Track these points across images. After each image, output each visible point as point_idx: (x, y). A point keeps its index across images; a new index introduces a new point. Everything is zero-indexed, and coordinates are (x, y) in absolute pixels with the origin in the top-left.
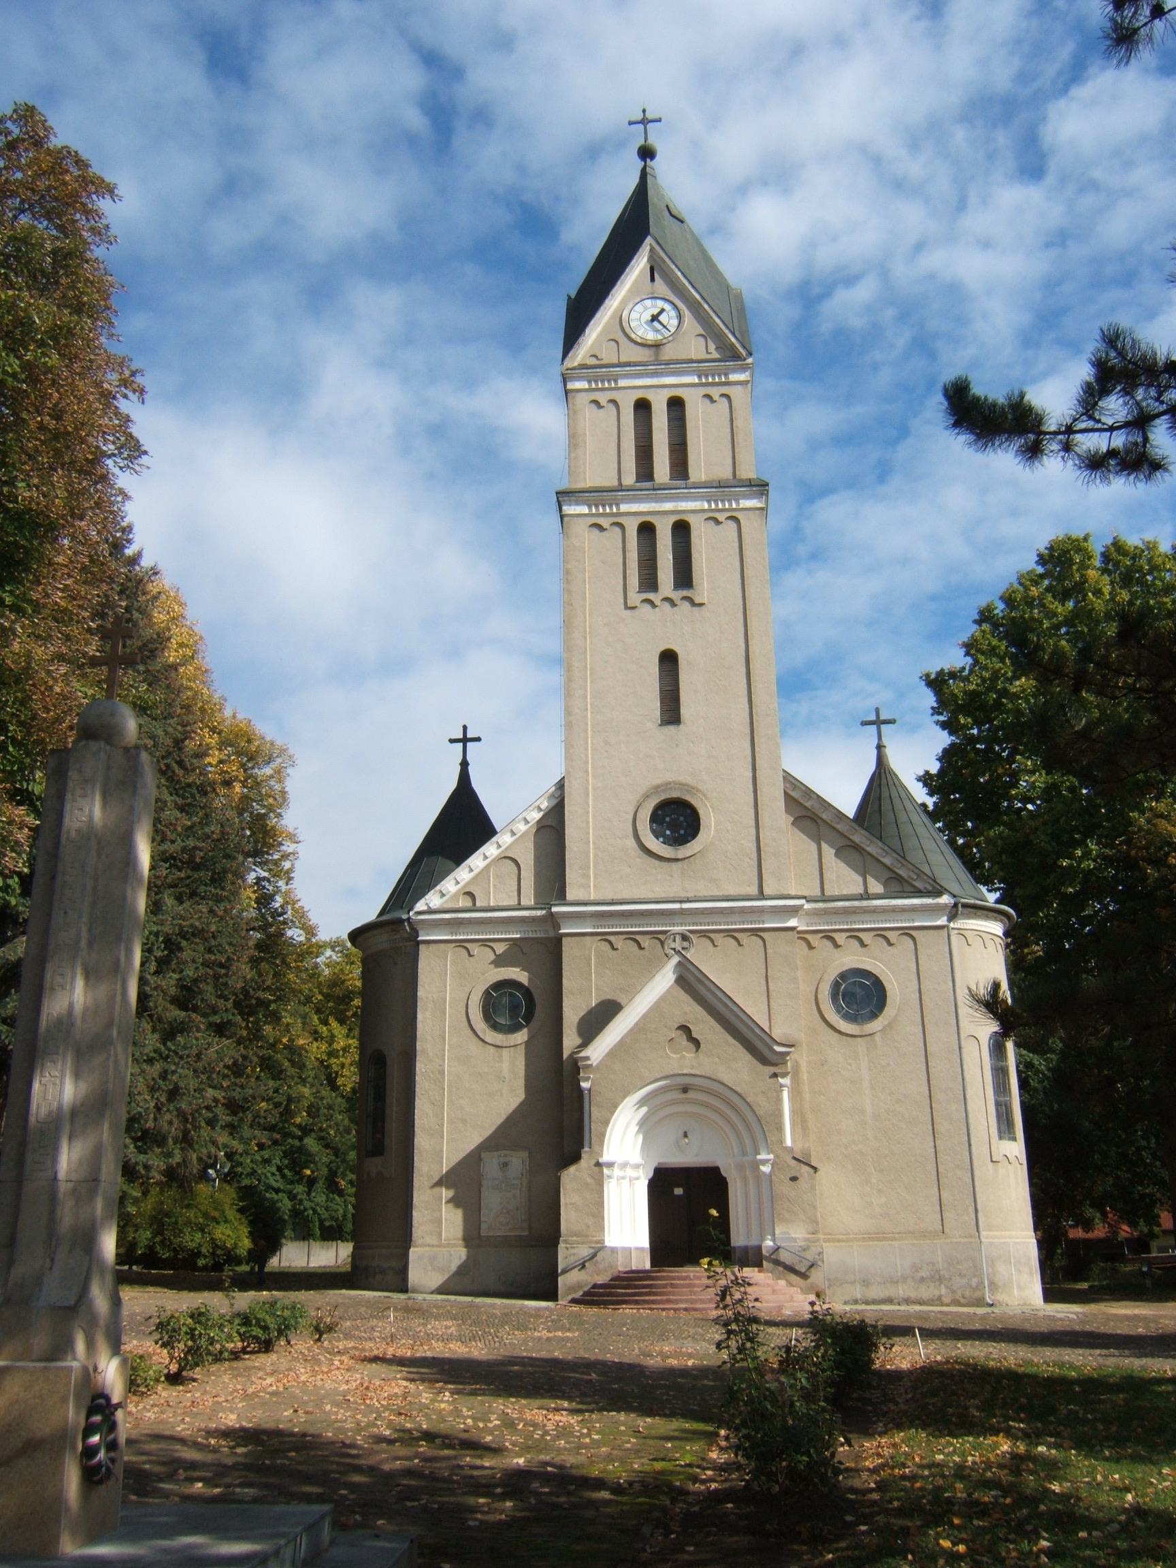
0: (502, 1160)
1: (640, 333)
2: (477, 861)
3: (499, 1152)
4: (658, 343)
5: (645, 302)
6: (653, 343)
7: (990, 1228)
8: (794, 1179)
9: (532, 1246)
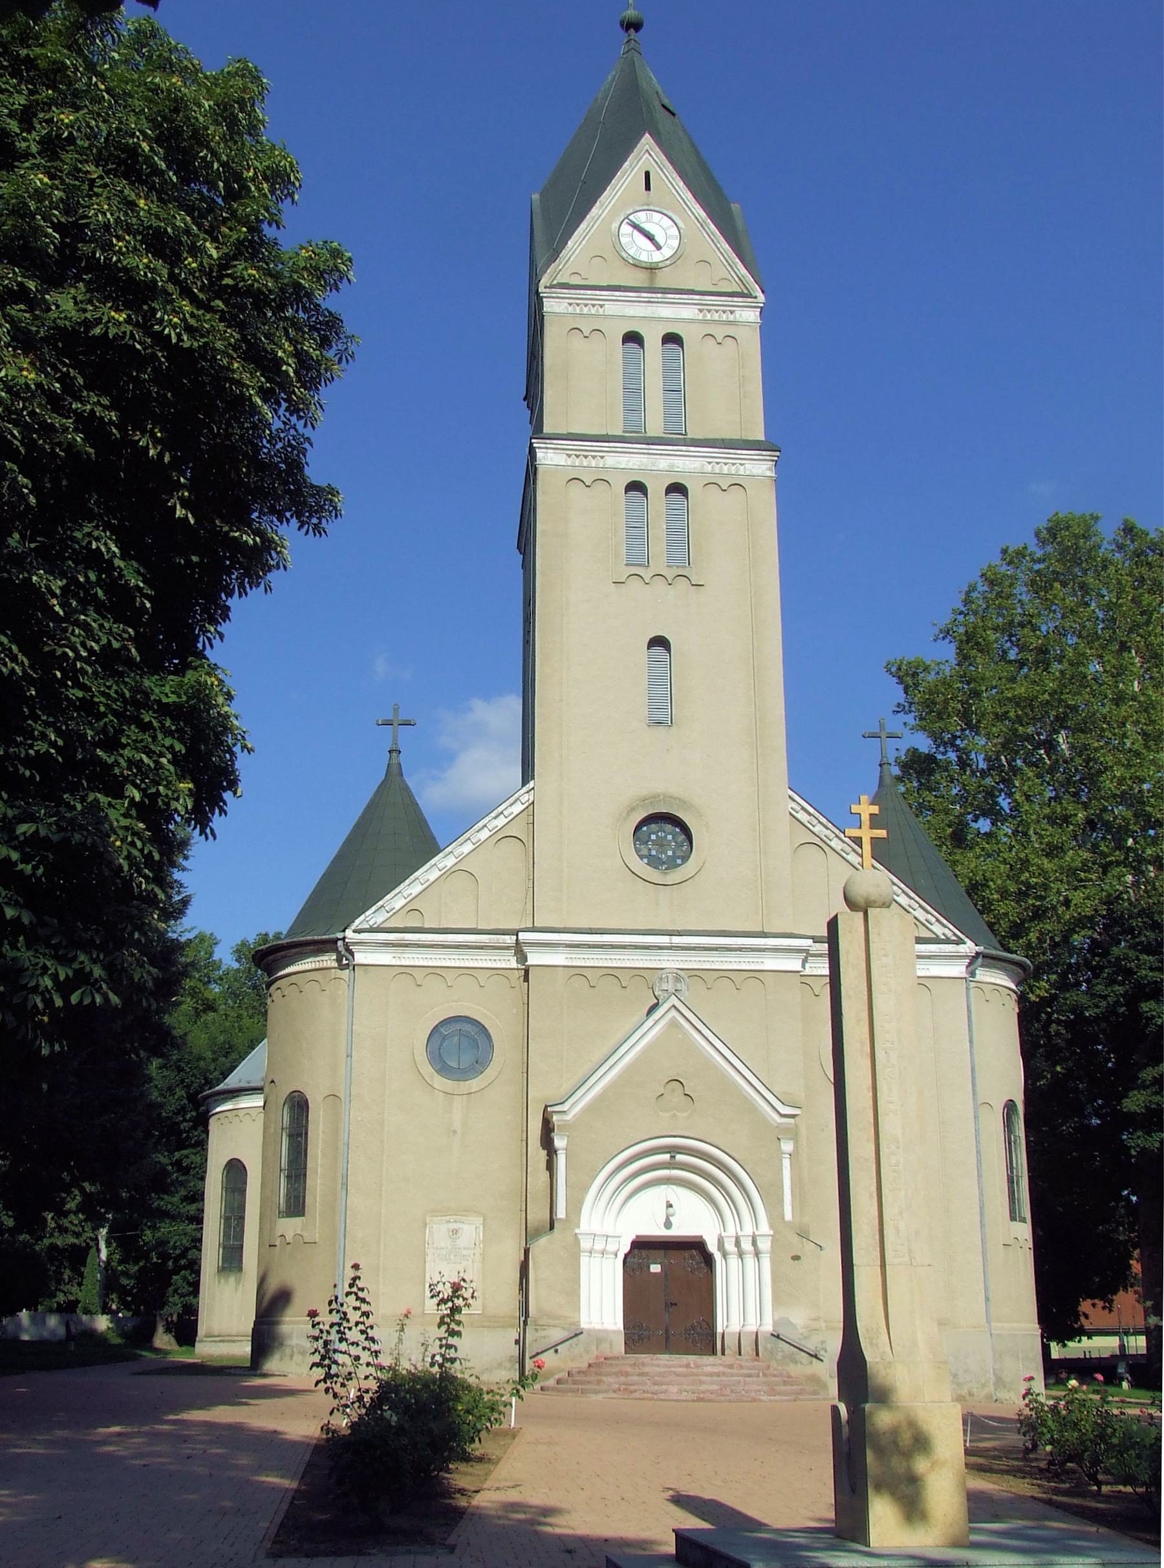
0: (452, 1226)
1: (631, 252)
2: (429, 873)
3: (447, 1218)
4: (653, 266)
5: (639, 214)
6: (648, 266)
7: (514, 1318)
8: (796, 1258)
9: (484, 1327)
